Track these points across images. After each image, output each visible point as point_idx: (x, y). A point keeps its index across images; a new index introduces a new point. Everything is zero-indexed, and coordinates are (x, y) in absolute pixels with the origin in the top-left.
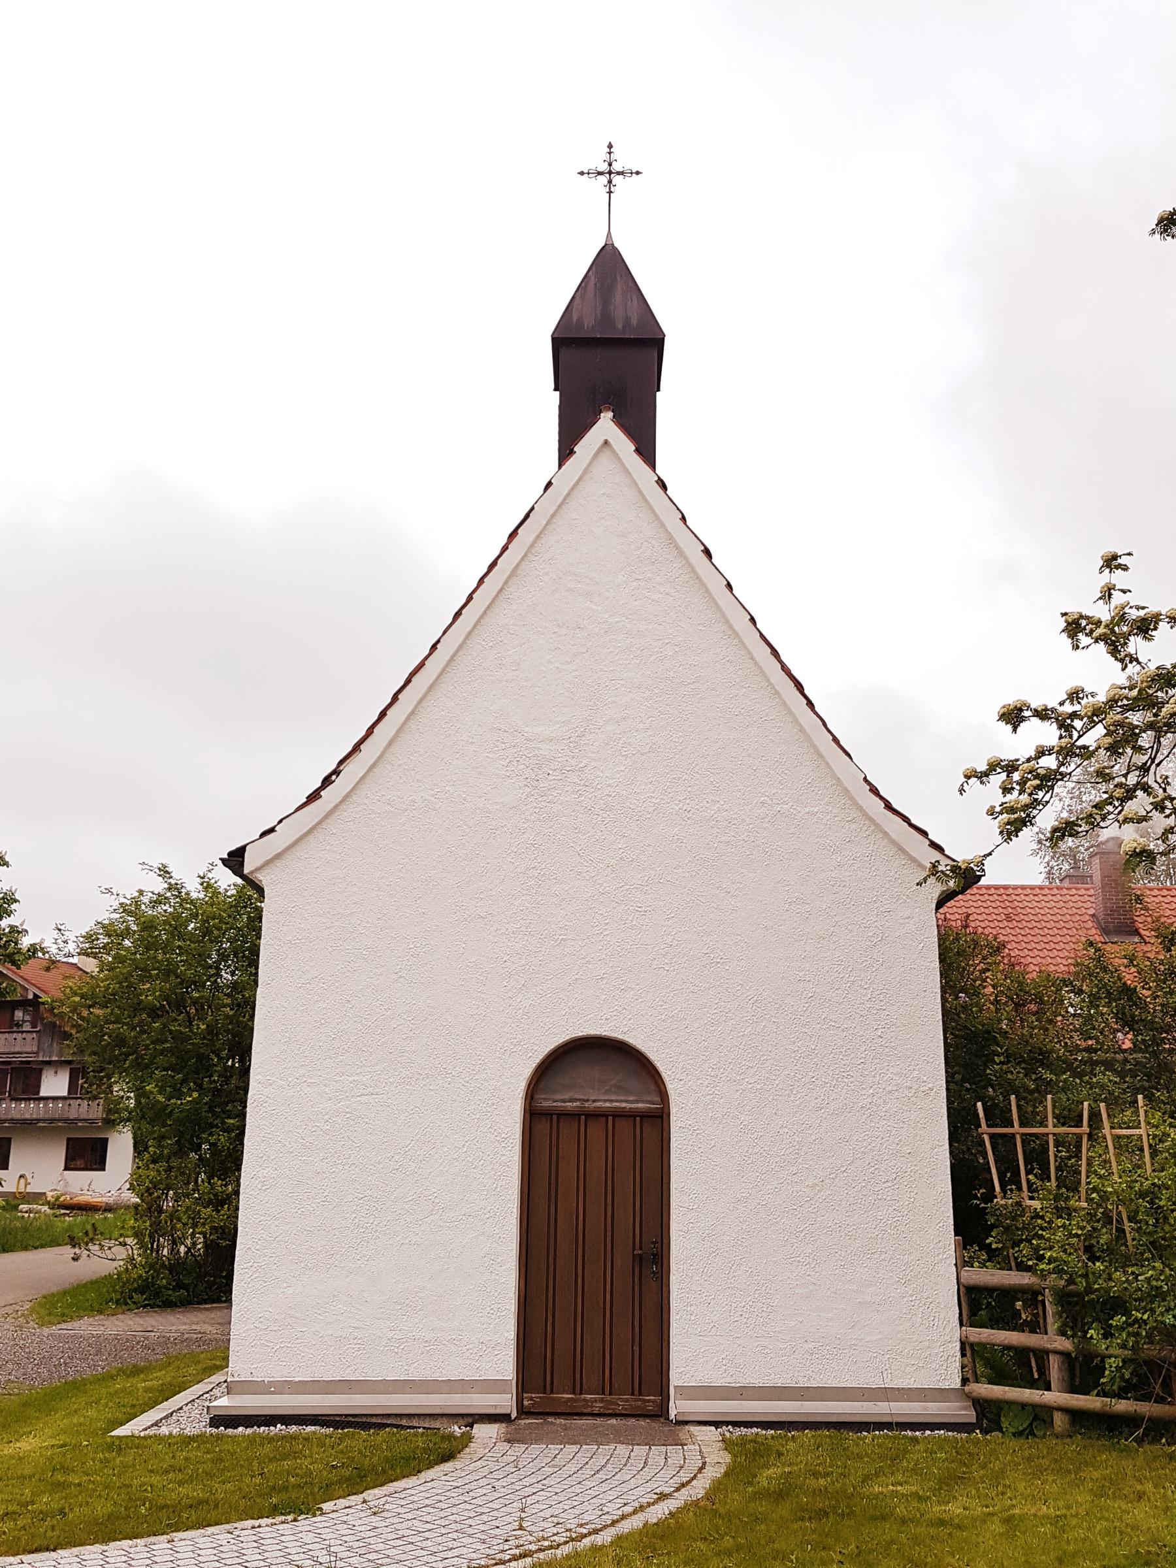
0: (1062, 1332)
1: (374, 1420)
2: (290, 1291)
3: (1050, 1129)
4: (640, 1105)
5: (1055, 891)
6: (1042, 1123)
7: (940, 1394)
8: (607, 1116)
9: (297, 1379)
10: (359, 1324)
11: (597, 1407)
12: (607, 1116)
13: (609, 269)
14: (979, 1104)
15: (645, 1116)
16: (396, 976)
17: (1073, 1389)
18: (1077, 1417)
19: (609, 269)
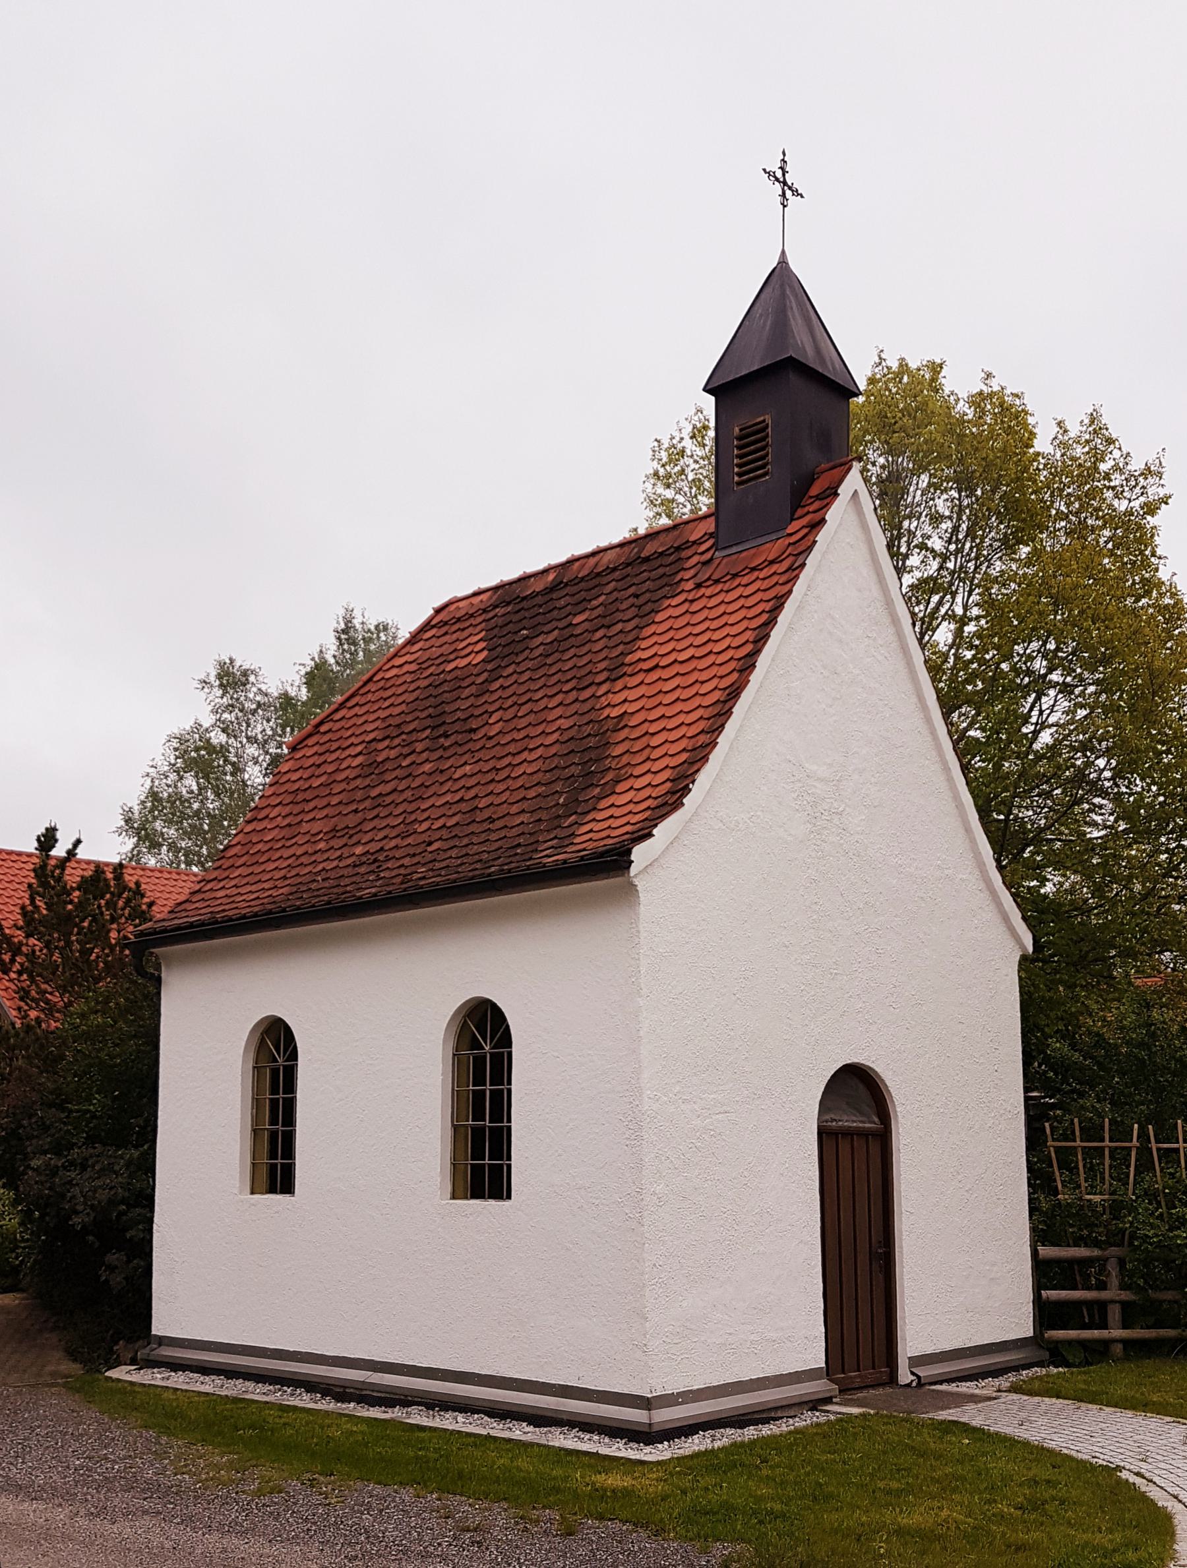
0: (1122, 1287)
1: (756, 1416)
2: (685, 1304)
3: (1078, 1143)
4: (867, 1125)
5: (175, 876)
6: (1103, 1140)
7: (809, 1375)
8: (852, 1135)
9: (695, 1388)
10: (732, 1331)
11: (858, 1382)
12: (852, 1135)
13: (782, 293)
14: (1136, 1126)
15: (863, 1134)
16: (734, 998)
17: (1124, 1328)
18: (1127, 1343)
19: (782, 293)
